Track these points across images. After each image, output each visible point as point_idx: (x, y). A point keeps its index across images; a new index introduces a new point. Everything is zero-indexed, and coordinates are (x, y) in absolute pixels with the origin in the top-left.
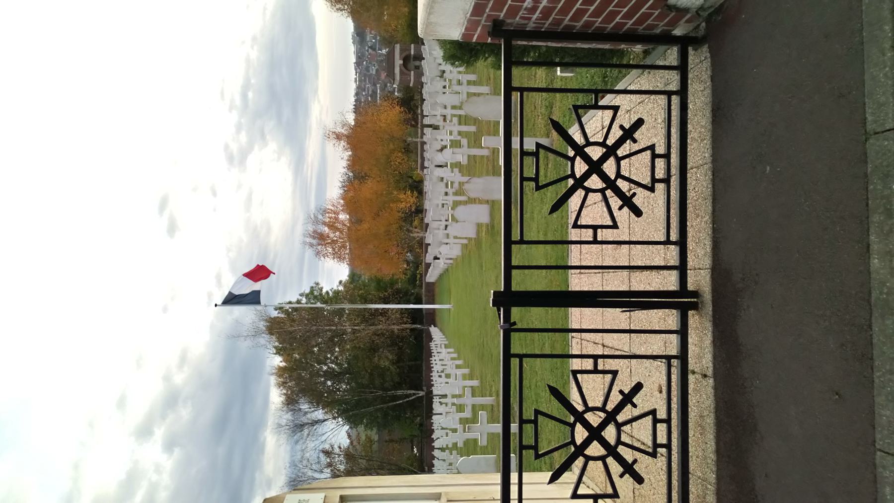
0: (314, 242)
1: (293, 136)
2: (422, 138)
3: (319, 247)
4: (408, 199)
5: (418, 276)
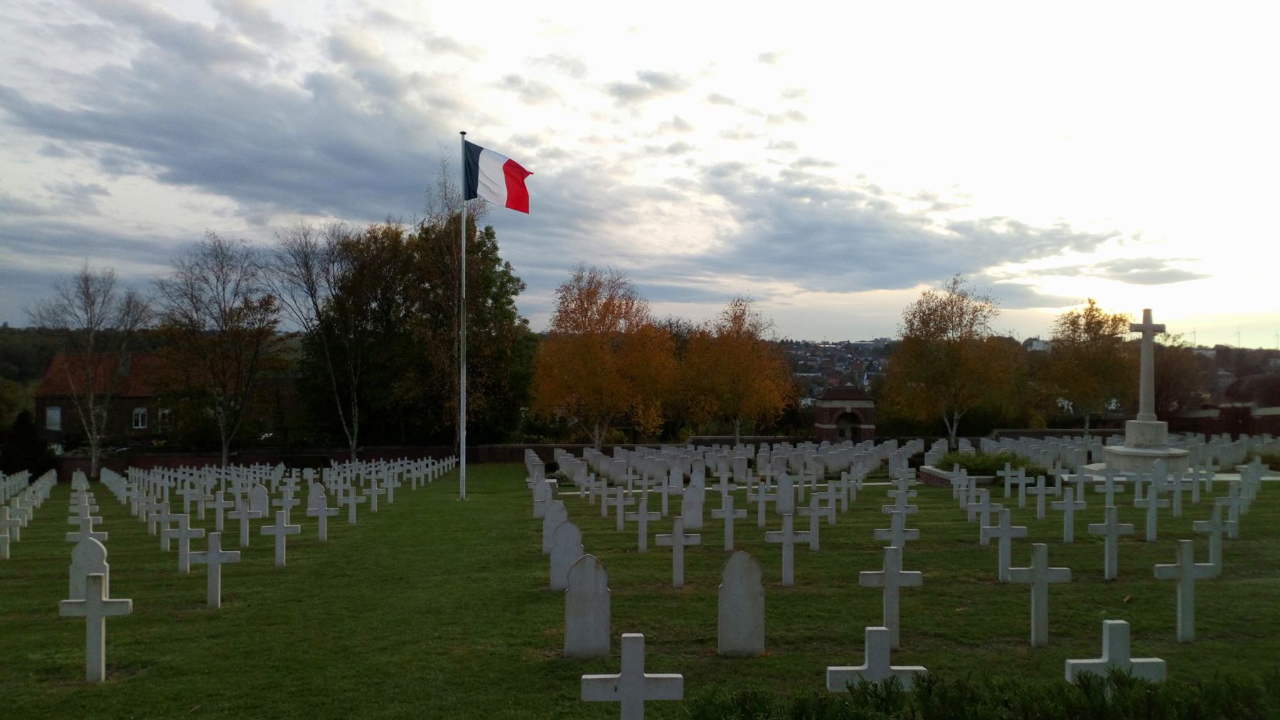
0: (584, 283)
1: (746, 258)
2: (741, 441)
3: (576, 291)
4: (653, 420)
5: (535, 437)
